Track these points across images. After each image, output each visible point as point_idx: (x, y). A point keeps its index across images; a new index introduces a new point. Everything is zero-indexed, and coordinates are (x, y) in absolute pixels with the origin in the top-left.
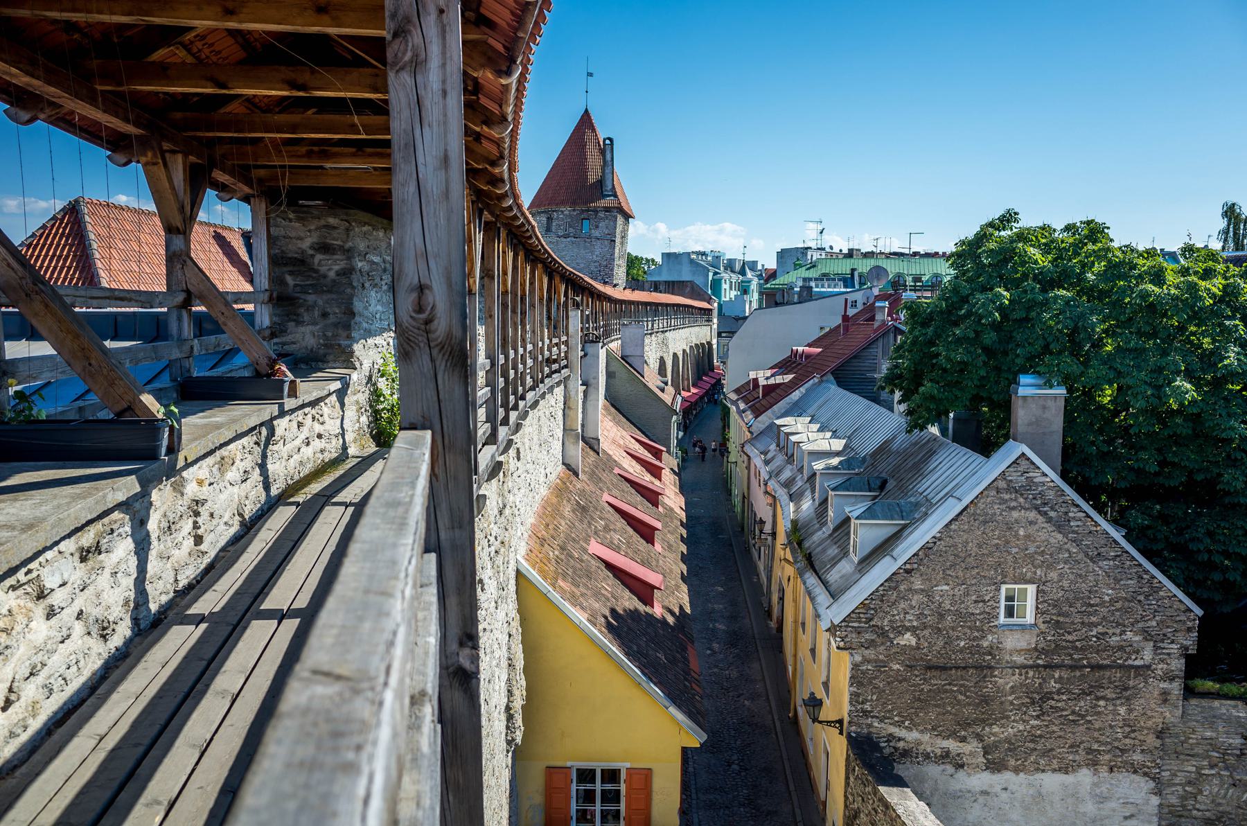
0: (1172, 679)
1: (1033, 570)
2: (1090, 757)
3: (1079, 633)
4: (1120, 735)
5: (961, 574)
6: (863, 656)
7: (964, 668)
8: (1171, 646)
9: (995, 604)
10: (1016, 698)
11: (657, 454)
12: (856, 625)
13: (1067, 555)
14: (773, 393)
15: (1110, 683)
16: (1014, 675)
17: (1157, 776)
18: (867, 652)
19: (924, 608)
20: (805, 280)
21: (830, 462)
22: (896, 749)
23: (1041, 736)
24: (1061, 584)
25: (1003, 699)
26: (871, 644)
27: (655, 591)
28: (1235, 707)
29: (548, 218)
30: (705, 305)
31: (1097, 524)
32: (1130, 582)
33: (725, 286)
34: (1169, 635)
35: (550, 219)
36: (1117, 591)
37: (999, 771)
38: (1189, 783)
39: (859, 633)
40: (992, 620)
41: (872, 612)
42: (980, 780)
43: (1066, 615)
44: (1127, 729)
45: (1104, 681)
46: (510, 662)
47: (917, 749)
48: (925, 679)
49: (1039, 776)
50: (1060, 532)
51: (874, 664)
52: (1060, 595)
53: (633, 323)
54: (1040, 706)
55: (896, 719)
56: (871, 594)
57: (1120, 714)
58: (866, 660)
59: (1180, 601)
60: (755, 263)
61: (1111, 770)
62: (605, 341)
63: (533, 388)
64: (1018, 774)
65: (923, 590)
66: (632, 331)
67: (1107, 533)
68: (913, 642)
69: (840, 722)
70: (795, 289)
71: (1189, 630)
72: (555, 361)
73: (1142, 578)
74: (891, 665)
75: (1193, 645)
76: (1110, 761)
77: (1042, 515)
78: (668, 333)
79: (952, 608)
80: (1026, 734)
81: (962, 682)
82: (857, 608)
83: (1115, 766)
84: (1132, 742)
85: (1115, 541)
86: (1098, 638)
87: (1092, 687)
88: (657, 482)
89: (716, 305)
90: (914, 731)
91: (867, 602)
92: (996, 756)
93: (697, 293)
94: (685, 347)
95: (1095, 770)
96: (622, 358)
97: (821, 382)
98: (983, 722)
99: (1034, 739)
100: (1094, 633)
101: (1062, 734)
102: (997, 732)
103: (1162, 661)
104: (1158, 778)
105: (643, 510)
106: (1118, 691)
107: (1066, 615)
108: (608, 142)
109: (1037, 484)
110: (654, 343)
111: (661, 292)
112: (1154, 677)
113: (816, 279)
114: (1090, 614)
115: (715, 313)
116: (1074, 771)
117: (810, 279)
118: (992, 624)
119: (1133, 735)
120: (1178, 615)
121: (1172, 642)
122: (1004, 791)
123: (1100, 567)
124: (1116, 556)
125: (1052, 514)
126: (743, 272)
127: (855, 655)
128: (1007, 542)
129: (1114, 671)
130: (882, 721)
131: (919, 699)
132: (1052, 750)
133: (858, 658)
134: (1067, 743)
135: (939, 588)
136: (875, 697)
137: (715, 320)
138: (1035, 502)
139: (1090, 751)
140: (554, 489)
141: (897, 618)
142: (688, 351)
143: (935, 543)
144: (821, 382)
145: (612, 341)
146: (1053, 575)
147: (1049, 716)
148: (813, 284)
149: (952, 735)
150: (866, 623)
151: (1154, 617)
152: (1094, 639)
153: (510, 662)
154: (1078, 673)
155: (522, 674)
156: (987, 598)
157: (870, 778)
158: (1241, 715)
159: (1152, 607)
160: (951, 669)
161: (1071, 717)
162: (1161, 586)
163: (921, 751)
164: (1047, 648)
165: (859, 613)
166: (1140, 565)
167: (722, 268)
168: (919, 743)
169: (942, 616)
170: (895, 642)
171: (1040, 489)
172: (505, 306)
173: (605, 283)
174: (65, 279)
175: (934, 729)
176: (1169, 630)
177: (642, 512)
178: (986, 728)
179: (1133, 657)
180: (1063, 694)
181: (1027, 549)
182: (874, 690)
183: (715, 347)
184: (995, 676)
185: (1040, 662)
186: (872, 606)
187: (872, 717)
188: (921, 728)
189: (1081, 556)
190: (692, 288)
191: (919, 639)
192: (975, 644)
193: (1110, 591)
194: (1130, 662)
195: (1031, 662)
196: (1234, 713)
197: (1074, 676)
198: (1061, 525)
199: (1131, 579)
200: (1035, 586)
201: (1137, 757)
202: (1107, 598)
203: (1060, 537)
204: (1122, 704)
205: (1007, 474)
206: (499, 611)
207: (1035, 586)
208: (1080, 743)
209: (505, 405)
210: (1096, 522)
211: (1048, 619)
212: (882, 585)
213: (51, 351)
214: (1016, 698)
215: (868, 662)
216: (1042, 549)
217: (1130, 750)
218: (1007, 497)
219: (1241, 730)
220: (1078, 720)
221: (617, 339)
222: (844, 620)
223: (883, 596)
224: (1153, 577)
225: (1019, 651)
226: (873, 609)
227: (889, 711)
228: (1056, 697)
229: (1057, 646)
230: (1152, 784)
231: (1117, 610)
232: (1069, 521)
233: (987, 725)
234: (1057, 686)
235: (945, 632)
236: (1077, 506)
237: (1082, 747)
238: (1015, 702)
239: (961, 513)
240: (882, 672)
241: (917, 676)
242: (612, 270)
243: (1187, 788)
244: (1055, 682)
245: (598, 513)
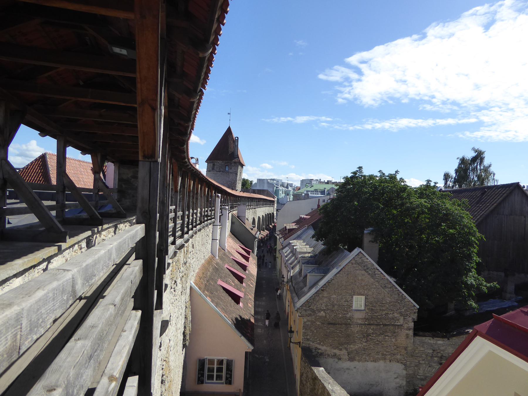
0: (410, 330)
1: (364, 291)
2: (383, 356)
3: (379, 313)
4: (393, 349)
5: (340, 292)
6: (307, 319)
7: (341, 324)
8: (409, 318)
9: (351, 302)
10: (358, 335)
11: (248, 253)
12: (305, 308)
13: (375, 286)
14: (291, 231)
15: (390, 330)
16: (358, 327)
17: (405, 363)
18: (309, 318)
19: (327, 303)
20: (307, 191)
21: (304, 255)
22: (318, 353)
23: (367, 349)
24: (373, 296)
25: (354, 335)
26: (310, 315)
27: (241, 298)
28: (430, 339)
29: (213, 165)
30: (272, 199)
31: (384, 276)
32: (395, 296)
33: (281, 192)
34: (408, 314)
35: (214, 165)
36: (391, 299)
37: (353, 361)
38: (416, 366)
39: (306, 311)
40: (350, 308)
41: (310, 304)
42: (347, 364)
43: (375, 307)
44: (395, 347)
45: (388, 330)
46: (186, 316)
47: (325, 353)
48: (328, 328)
49: (366, 363)
50: (372, 278)
51: (311, 322)
52: (373, 300)
53: (242, 204)
54: (366, 338)
55: (318, 342)
56: (310, 298)
57: (393, 342)
58: (308, 321)
59: (412, 303)
60: (292, 184)
61: (390, 361)
62: (231, 210)
63: (199, 224)
64: (359, 362)
65: (327, 297)
66: (242, 207)
67: (388, 279)
68: (324, 314)
69: (300, 343)
70: (303, 195)
71: (415, 313)
72: (209, 216)
73: (399, 295)
74: (317, 322)
75: (416, 318)
76: (390, 358)
77: (367, 273)
78: (256, 209)
79: (337, 303)
80: (362, 348)
81: (340, 329)
82: (305, 302)
83: (391, 360)
84: (397, 351)
85: (391, 282)
86: (385, 315)
87: (383, 332)
88: (247, 263)
89: (276, 199)
90: (324, 346)
91: (308, 300)
92: (352, 355)
93: (268, 194)
94: (263, 214)
95: (385, 361)
96: (237, 217)
97: (308, 228)
98: (348, 344)
99: (364, 349)
100: (384, 313)
101: (374, 348)
102: (353, 347)
103: (406, 323)
104: (406, 364)
105: (240, 271)
106: (392, 333)
107: (375, 307)
108: (236, 138)
109: (365, 262)
110: (251, 212)
111: (255, 193)
112: (404, 329)
113: (311, 191)
114: (382, 306)
115: (276, 202)
116: (378, 361)
117: (309, 191)
118: (350, 309)
119: (397, 349)
120: (411, 308)
121: (410, 317)
122: (354, 368)
123: (386, 291)
124: (391, 287)
125: (370, 272)
126: (287, 187)
127: (304, 319)
128: (355, 281)
129: (391, 326)
130: (313, 342)
131: (326, 335)
132: (370, 354)
133: (305, 320)
134: (375, 351)
135: (333, 296)
136: (311, 334)
137: (276, 205)
138: (364, 268)
139: (383, 354)
140: (207, 261)
141: (319, 306)
142: (264, 216)
143: (332, 281)
144: (308, 228)
145: (234, 211)
146: (370, 293)
147: (369, 341)
148: (309, 193)
149: (337, 348)
150: (308, 308)
151: (404, 308)
152: (384, 315)
153: (186, 316)
154: (379, 327)
155: (190, 322)
156: (349, 300)
157: (307, 361)
158: (432, 342)
159: (403, 305)
160: (336, 324)
161: (377, 342)
162: (405, 298)
163: (326, 353)
164: (368, 318)
165: (306, 304)
166: (399, 290)
167: (279, 186)
168: (326, 351)
169: (334, 306)
170: (318, 315)
171: (366, 264)
172: (189, 196)
173: (233, 189)
174: (31, 180)
175: (331, 346)
176: (408, 313)
177: (240, 273)
178: (349, 346)
179: (397, 322)
180: (374, 334)
181: (361, 284)
182: (311, 331)
183: (275, 215)
184: (351, 327)
185: (366, 323)
186: (310, 302)
187: (310, 341)
188: (326, 345)
189: (380, 287)
190: (267, 192)
191: (326, 314)
192: (344, 316)
193: (389, 299)
194: (396, 323)
195: (363, 323)
196: (429, 341)
197: (378, 328)
198: (373, 276)
199: (395, 295)
200: (364, 296)
201: (399, 357)
202: (388, 301)
203: (372, 280)
204: (393, 338)
205: (355, 258)
206: (182, 296)
207: (364, 296)
208: (380, 352)
209: (188, 227)
210: (384, 275)
211: (369, 308)
212: (314, 294)
213: (26, 206)
214: (358, 335)
215: (309, 321)
216: (367, 284)
217: (396, 354)
218: (355, 266)
219: (432, 347)
220: (379, 343)
221: (236, 210)
222: (301, 307)
223: (314, 298)
224: (403, 294)
225: (359, 319)
226: (311, 303)
227: (316, 339)
228: (372, 335)
229: (372, 317)
230: (403, 366)
231: (391, 305)
232: (375, 275)
233: (349, 345)
234: (372, 331)
235: (334, 312)
236: (378, 270)
237: (380, 353)
238: (358, 336)
239: (340, 271)
240: (313, 325)
241: (325, 327)
242: (236, 185)
243: (415, 368)
244: (371, 330)
245: (223, 271)
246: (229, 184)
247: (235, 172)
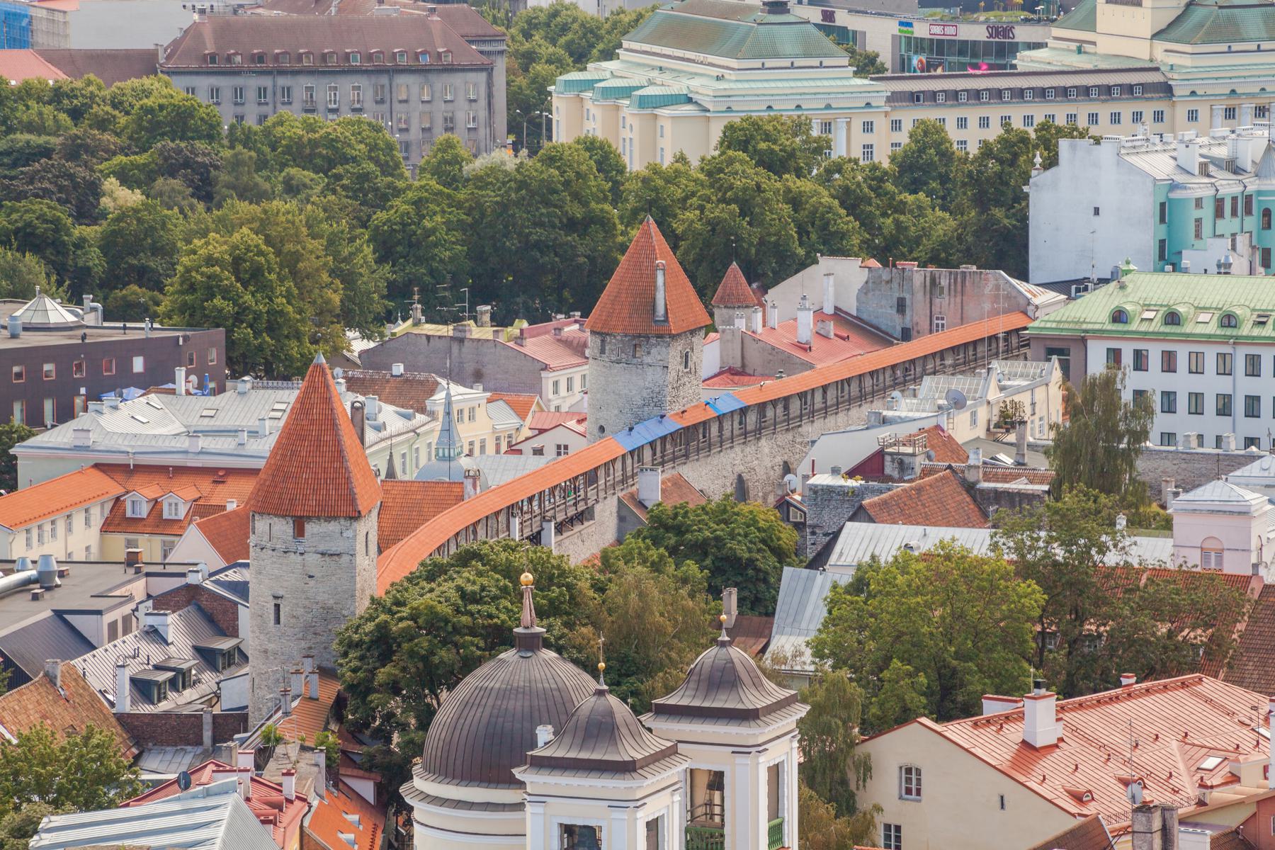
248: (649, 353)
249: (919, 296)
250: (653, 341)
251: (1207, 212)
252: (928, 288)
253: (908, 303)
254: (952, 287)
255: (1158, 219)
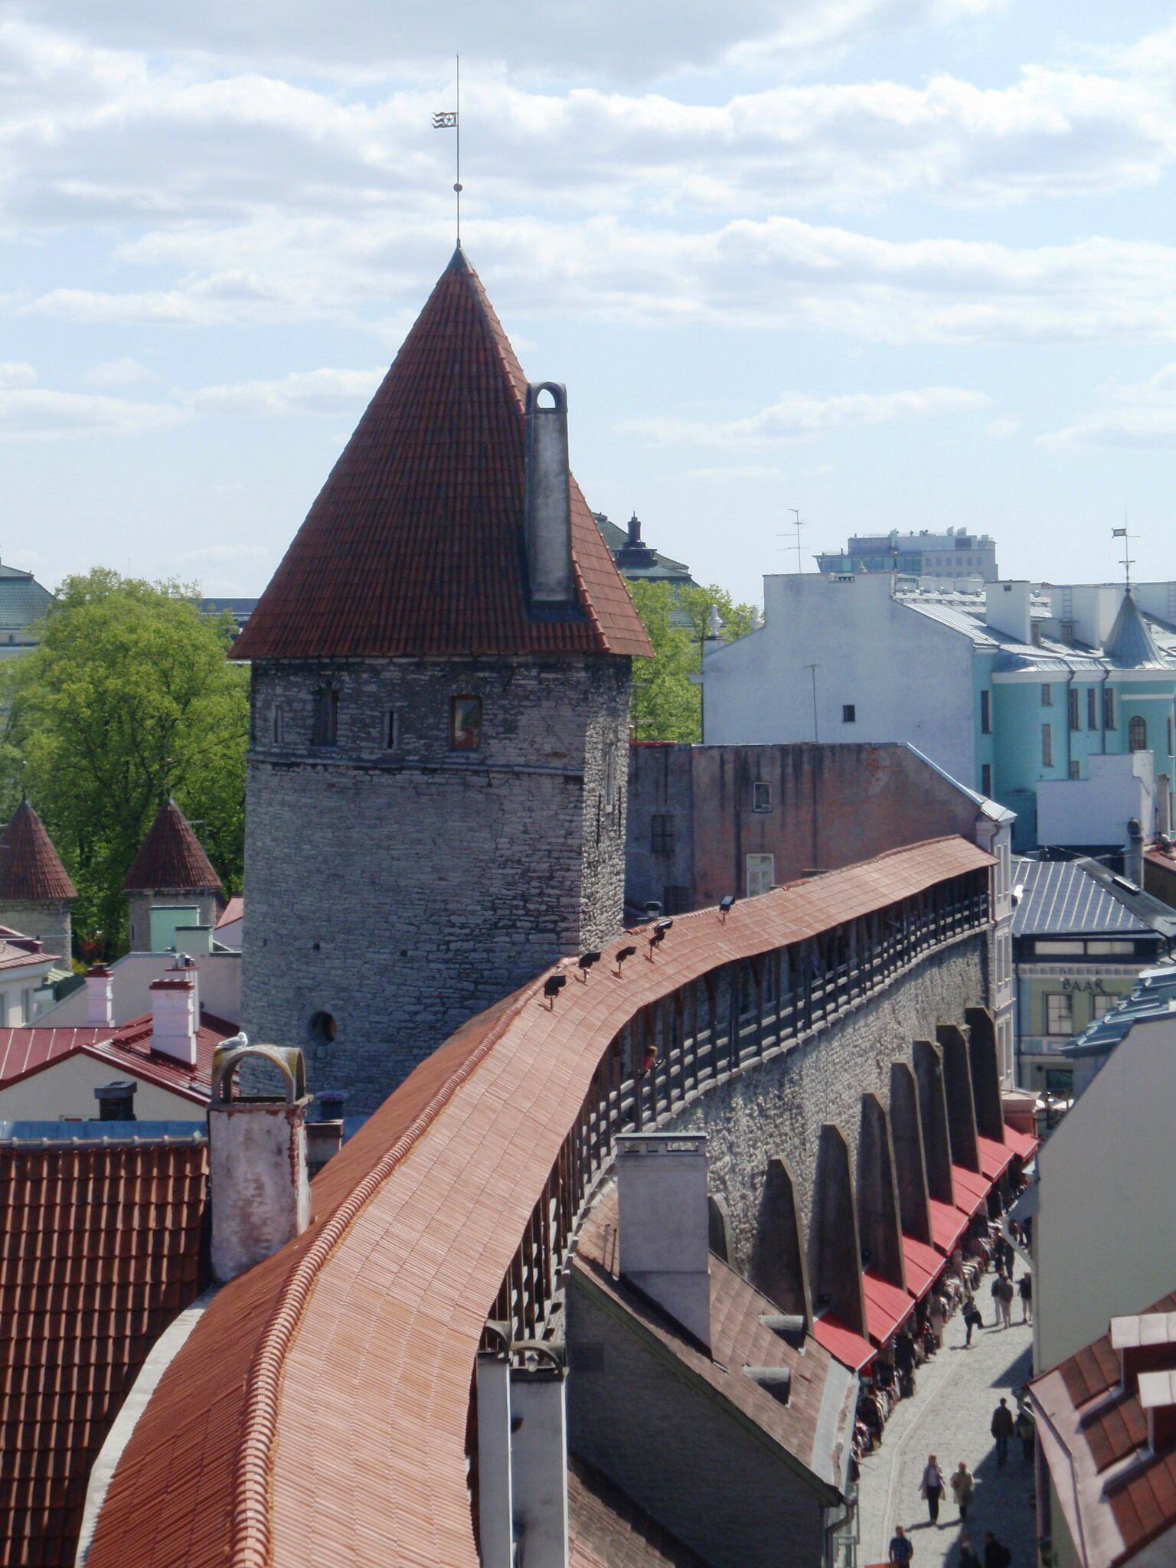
29: (319, 693)
35: (327, 698)
142: (851, 1136)
183: (1004, 1024)
246: (497, 888)
247: (557, 763)
248: (511, 728)
249: (709, 809)
250: (527, 680)
251: (1056, 716)
252: (730, 787)
253: (679, 825)
254: (790, 785)
255: (980, 727)
